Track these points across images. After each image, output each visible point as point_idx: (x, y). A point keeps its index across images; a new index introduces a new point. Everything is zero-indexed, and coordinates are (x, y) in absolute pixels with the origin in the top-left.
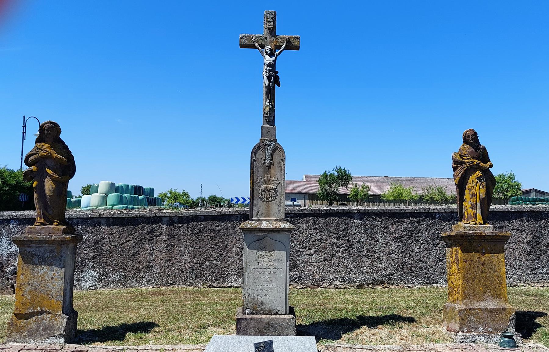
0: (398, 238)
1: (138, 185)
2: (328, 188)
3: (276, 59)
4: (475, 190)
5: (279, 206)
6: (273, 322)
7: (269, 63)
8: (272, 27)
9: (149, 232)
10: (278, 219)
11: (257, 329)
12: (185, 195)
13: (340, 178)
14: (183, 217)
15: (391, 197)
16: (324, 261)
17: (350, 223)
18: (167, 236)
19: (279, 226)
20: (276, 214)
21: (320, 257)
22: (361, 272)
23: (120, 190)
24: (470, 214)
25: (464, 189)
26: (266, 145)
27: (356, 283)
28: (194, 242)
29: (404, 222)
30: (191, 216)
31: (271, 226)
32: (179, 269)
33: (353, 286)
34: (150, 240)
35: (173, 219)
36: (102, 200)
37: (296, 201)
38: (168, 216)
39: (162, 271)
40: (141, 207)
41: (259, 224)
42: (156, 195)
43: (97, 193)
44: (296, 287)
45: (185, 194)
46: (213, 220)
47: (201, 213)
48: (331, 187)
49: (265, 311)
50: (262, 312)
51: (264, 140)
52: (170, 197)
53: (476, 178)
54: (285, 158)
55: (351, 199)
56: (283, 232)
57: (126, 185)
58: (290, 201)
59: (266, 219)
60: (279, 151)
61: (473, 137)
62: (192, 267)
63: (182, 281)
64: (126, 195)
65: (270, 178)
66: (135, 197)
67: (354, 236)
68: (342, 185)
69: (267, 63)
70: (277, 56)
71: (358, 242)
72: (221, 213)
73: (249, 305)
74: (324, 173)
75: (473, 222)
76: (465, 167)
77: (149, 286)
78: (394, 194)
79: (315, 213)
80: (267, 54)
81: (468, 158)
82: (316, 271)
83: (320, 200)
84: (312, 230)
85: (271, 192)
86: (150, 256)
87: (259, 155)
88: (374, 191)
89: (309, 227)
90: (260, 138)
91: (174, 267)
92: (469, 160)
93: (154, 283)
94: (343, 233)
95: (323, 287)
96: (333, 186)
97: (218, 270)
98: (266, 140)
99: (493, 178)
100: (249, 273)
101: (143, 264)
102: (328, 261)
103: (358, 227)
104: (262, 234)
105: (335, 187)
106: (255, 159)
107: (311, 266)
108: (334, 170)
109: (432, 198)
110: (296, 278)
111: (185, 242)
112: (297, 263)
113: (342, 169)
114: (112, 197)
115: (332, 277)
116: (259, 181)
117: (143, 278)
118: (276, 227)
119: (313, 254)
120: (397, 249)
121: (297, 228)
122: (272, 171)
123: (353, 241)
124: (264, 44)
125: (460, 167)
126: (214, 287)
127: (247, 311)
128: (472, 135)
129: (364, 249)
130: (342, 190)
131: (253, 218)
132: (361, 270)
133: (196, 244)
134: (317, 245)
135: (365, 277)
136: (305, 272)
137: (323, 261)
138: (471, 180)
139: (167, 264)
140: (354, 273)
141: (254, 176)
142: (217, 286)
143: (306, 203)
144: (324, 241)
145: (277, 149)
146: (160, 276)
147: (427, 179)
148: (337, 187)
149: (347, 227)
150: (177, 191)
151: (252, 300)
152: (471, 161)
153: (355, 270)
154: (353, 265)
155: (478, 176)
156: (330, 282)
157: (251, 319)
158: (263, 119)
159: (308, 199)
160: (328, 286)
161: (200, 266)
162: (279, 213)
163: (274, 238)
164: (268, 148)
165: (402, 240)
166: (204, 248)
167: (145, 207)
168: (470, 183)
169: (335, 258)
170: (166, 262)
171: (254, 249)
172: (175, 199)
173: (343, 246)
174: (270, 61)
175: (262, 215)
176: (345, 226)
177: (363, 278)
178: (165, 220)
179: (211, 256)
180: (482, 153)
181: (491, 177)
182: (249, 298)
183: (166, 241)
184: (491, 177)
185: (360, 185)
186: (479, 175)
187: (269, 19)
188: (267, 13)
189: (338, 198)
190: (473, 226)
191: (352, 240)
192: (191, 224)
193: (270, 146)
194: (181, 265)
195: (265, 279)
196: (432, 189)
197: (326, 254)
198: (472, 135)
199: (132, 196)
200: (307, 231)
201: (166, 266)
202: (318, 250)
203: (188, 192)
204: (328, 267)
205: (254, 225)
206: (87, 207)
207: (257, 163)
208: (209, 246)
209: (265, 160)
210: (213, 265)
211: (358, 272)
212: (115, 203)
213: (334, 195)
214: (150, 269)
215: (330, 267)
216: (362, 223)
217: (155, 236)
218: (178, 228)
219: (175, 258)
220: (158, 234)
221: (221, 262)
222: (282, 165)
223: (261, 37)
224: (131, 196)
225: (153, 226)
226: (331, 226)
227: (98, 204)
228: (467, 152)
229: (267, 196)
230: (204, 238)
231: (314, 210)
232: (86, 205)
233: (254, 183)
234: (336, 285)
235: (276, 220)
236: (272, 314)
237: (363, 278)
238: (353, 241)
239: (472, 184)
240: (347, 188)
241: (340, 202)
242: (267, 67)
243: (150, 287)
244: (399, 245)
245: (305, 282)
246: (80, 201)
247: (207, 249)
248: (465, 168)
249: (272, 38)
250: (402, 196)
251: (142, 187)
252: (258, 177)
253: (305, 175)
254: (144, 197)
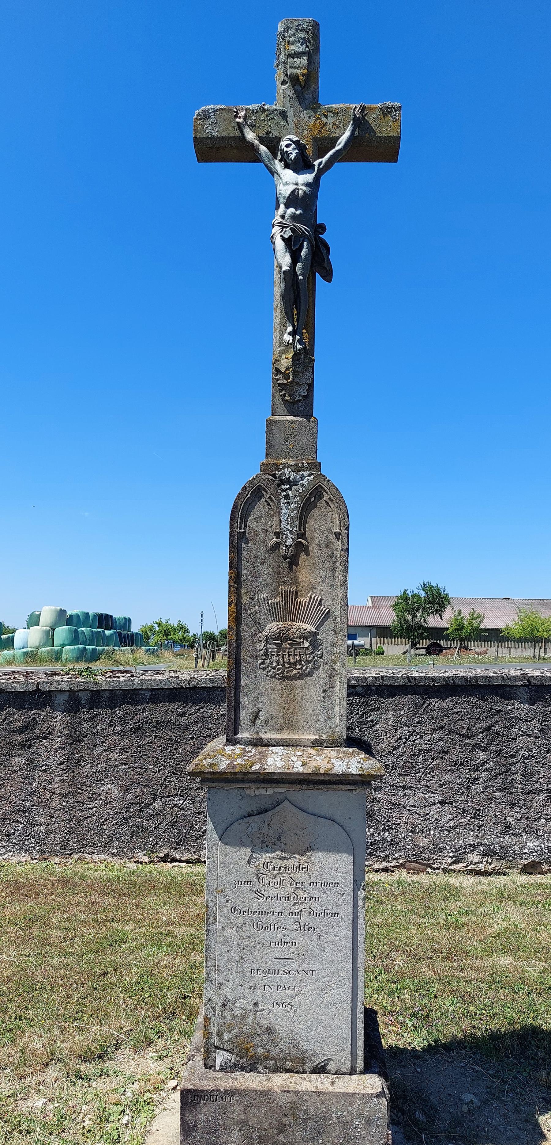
1: (104, 612)
2: (409, 617)
3: (317, 179)
5: (327, 694)
6: (311, 1108)
7: (293, 192)
8: (306, 71)
9: (23, 728)
10: (324, 737)
11: (254, 1128)
12: (181, 628)
13: (430, 601)
14: (101, 694)
15: (518, 633)
16: (441, 802)
17: (506, 710)
18: (66, 738)
19: (328, 766)
20: (318, 721)
21: (430, 794)
22: (533, 833)
23: (75, 620)
26: (282, 482)
27: (522, 859)
28: (127, 752)
30: (120, 690)
31: (298, 768)
32: (94, 815)
33: (514, 867)
34: (24, 746)
35: (78, 696)
36: (45, 637)
37: (356, 639)
38: (65, 691)
39: (54, 819)
40: (108, 648)
41: (257, 757)
42: (135, 628)
43: (39, 625)
44: (371, 865)
45: (182, 627)
46: (172, 701)
47: (142, 684)
48: (414, 616)
49: (282, 1060)
50: (270, 1063)
51: (276, 466)
52: (158, 632)
54: (347, 529)
55: (451, 636)
56: (341, 787)
57: (84, 613)
59: (284, 739)
60: (327, 503)
62: (123, 811)
63: (99, 845)
64: (83, 629)
65: (296, 597)
66: (98, 631)
67: (515, 744)
68: (432, 613)
69: (285, 191)
70: (321, 172)
71: (525, 759)
72: (189, 684)
73: (226, 1036)
74: (402, 593)
77: (23, 854)
78: (525, 627)
79: (416, 686)
80: (287, 166)
82: (420, 826)
83: (396, 636)
84: (409, 727)
85: (299, 644)
86: (26, 784)
87: (257, 519)
88: (488, 624)
89: (403, 720)
90: (264, 460)
91: (82, 810)
93: (34, 847)
94: (487, 735)
95: (438, 866)
96: (419, 614)
97: (184, 820)
98: (281, 467)
100: (223, 928)
101: (10, 802)
102: (449, 803)
103: (527, 720)
104: (270, 792)
105: (421, 616)
106: (244, 533)
107: (407, 813)
108: (420, 588)
110: (372, 844)
111: (106, 751)
112: (372, 806)
113: (433, 587)
114: (62, 632)
115: (461, 842)
116: (257, 607)
117: (9, 835)
118: (318, 768)
119: (412, 785)
121: (372, 721)
122: (304, 573)
123: (513, 756)
124: (278, 135)
126: (175, 860)
127: (220, 1058)
129: (542, 774)
130: (433, 621)
131: (239, 736)
132: (533, 825)
133: (132, 756)
134: (422, 764)
135: (544, 843)
136: (393, 829)
137: (438, 803)
139: (64, 804)
140: (515, 834)
141: (243, 591)
142: (182, 859)
144: (441, 755)
145: (321, 497)
146: (49, 832)
148: (424, 615)
149: (497, 722)
150: (169, 622)
151: (237, 1021)
153: (518, 827)
154: (512, 814)
156: (457, 856)
157: (232, 1093)
158: (273, 395)
160: (451, 864)
161: (141, 811)
162: (329, 717)
163: (310, 808)
164: (290, 493)
166: (150, 767)
167: (115, 648)
169: (468, 796)
170: (63, 799)
171: (241, 844)
172: (166, 634)
173: (487, 766)
174: (297, 184)
175: (271, 722)
176: (492, 718)
177: (539, 848)
178: (60, 699)
179: (166, 786)
182: (227, 1014)
183: (62, 748)
185: (466, 613)
187: (293, 47)
188: (288, 28)
189: (426, 634)
191: (510, 752)
192: (120, 710)
193: (297, 487)
194: (96, 805)
195: (280, 950)
197: (445, 785)
199: (93, 630)
200: (396, 730)
201: (64, 809)
202: (426, 775)
203: (185, 624)
204: (451, 817)
205: (239, 761)
206: (23, 648)
207: (251, 545)
208: (163, 763)
209: (278, 535)
210: (172, 808)
211: (526, 832)
212: (66, 643)
213: (419, 629)
214: (27, 814)
215: (456, 817)
216: (535, 711)
217: (37, 738)
218: (90, 719)
219: (82, 790)
220: (44, 733)
221: (190, 802)
222: (338, 553)
223: (267, 113)
224: (92, 631)
225: (32, 712)
226: (457, 717)
227: (40, 642)
229: (286, 658)
230: (151, 743)
231: (415, 678)
232: (21, 645)
233: (243, 615)
234: (471, 864)
235: (317, 744)
236: (305, 1072)
237: (539, 848)
238: (513, 756)
240: (441, 618)
241: (429, 640)
242: (287, 206)
243: (25, 859)
245: (394, 855)
246: (13, 637)
247: (157, 769)
249: (304, 114)
250: (538, 632)
251: (111, 616)
252: (256, 592)
253: (371, 597)
254: (115, 632)
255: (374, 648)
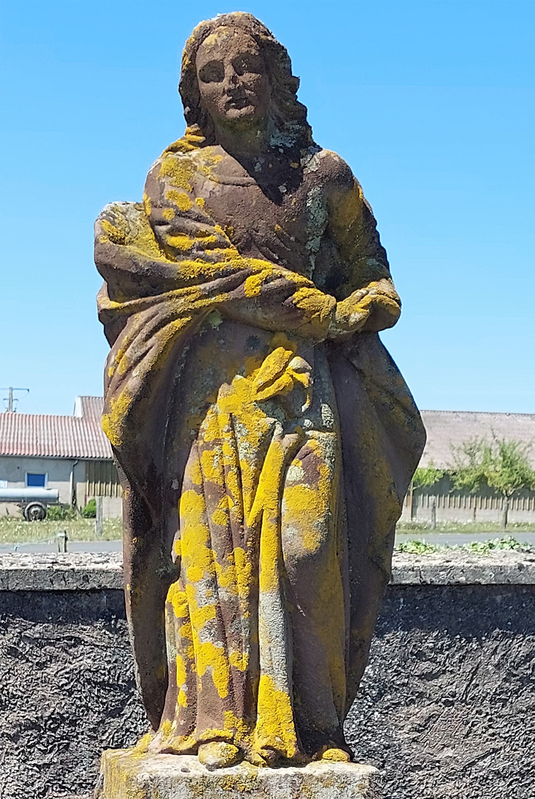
0: (39, 728)
4: (247, 498)
24: (207, 677)
25: (175, 486)
29: (78, 641)
53: (259, 403)
58: (23, 484)
61: (248, 77)
75: (218, 739)
76: (174, 317)
81: (201, 248)
92: (208, 260)
99: (405, 409)
109: (482, 479)
120: (36, 786)
125: (141, 316)
128: (233, 63)
138: (224, 421)
143: (77, 492)
147: (479, 416)
152: (222, 265)
155: (270, 391)
159: (84, 478)
165: (62, 738)
168: (218, 442)
180: (320, 216)
181: (387, 400)
184: (387, 400)
186: (285, 379)
190: (220, 772)
196: (483, 449)
198: (233, 63)
228: (200, 201)
239: (227, 448)
244: (47, 765)
248: (177, 323)
255: (80, 503)
